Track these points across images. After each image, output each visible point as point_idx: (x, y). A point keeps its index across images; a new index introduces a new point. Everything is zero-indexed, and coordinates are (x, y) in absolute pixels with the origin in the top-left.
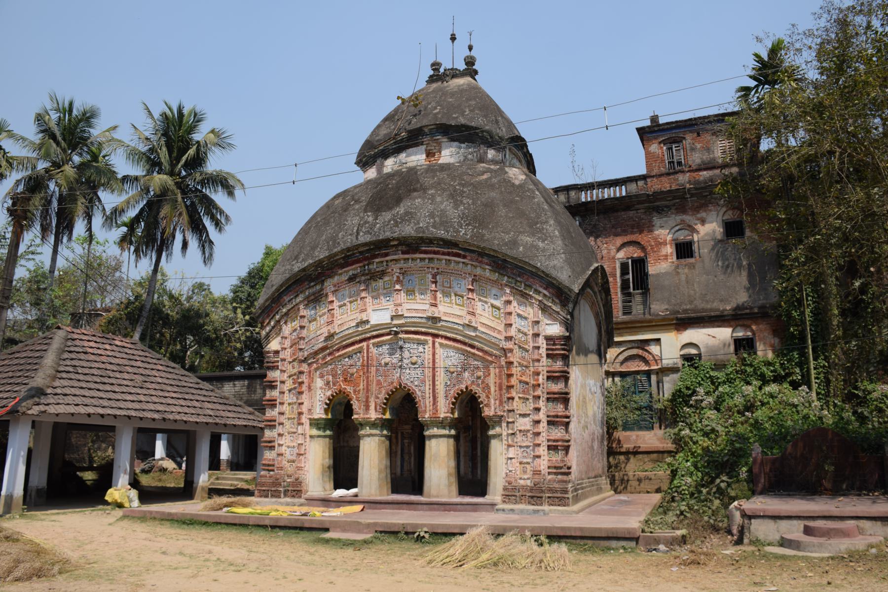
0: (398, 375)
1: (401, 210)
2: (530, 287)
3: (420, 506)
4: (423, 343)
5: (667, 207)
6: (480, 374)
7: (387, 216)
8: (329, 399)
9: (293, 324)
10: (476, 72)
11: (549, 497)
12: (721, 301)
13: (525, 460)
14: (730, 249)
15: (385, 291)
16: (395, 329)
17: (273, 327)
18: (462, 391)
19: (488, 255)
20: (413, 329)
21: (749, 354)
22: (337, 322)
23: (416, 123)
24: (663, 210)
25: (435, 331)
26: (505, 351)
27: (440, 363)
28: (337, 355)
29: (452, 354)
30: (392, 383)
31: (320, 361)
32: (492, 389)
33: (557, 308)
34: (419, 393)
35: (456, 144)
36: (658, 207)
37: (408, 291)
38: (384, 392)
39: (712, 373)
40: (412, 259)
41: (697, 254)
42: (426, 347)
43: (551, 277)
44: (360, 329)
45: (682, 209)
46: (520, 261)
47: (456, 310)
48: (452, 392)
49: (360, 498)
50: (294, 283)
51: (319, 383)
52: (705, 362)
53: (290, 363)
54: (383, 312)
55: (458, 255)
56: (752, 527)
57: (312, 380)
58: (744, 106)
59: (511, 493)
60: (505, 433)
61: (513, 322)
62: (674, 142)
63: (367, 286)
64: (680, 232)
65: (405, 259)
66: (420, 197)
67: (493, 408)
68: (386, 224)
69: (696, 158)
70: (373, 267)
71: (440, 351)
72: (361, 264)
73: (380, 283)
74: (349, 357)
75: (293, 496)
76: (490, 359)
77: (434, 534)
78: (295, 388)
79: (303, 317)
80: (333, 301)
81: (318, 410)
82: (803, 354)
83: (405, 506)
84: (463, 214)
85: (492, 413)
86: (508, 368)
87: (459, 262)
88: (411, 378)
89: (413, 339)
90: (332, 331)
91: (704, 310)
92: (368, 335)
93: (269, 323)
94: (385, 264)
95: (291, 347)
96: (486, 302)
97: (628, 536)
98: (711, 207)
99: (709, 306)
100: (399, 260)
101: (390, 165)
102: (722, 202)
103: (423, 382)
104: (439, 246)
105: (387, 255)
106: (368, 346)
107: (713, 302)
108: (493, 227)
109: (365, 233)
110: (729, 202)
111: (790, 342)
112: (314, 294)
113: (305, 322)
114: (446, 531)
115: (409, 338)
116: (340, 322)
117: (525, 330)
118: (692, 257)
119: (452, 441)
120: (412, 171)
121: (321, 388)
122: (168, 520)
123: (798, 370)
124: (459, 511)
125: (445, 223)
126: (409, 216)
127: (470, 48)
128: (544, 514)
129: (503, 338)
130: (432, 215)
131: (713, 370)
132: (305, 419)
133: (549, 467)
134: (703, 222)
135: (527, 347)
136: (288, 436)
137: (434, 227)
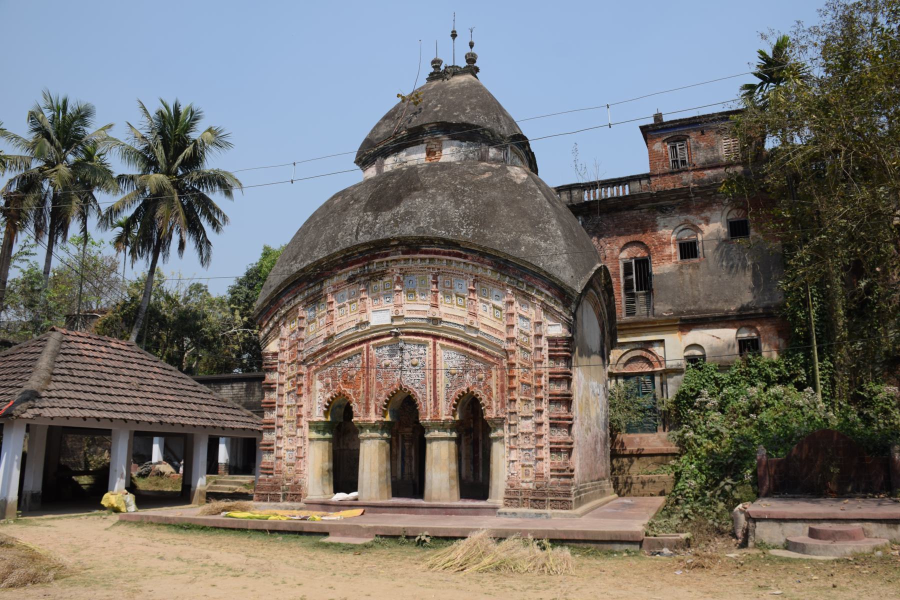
0: (398, 377)
1: (401, 209)
2: (532, 287)
3: (421, 510)
4: (424, 345)
5: (670, 206)
6: (482, 375)
7: (387, 215)
8: (329, 402)
9: (292, 325)
10: (477, 70)
11: (552, 501)
12: (726, 301)
13: (527, 463)
14: (734, 249)
15: (385, 292)
16: (395, 330)
17: (272, 329)
18: (463, 393)
19: (489, 255)
20: (413, 330)
21: (754, 355)
22: (336, 324)
23: (416, 122)
24: (666, 210)
25: (436, 332)
26: (507, 352)
27: (441, 365)
28: (337, 356)
29: (453, 356)
30: (393, 385)
31: (319, 363)
32: (494, 391)
33: (559, 309)
34: (420, 396)
35: (457, 142)
36: (662, 206)
37: (408, 292)
38: (384, 394)
39: (716, 375)
40: (413, 260)
41: (701, 254)
42: (427, 348)
43: (553, 278)
44: (360, 330)
45: (686, 208)
46: (522, 261)
47: (458, 311)
48: (453, 394)
49: (359, 502)
50: (294, 283)
51: (318, 385)
52: (710, 363)
53: (289, 365)
54: (383, 313)
55: (459, 255)
56: (757, 530)
57: (311, 382)
58: (749, 103)
59: (514, 497)
60: (506, 436)
61: (514, 323)
62: (678, 141)
63: (367, 287)
64: (684, 232)
65: (405, 260)
66: (420, 196)
67: (495, 411)
68: (385, 224)
69: (700, 157)
70: (373, 267)
71: (441, 353)
72: (361, 265)
73: (380, 284)
74: (348, 359)
75: (293, 500)
76: (491, 360)
77: (436, 538)
78: (294, 390)
79: (302, 318)
80: (332, 302)
81: (317, 413)
82: (808, 355)
83: (406, 509)
84: (465, 213)
85: (493, 416)
86: (510, 370)
87: (460, 263)
88: (412, 380)
89: (414, 341)
90: (331, 333)
91: (708, 311)
92: (368, 337)
93: (267, 325)
94: (385, 264)
95: (290, 349)
96: (488, 303)
97: (631, 539)
98: (715, 207)
99: (713, 307)
100: (400, 260)
101: (390, 163)
102: (726, 201)
103: (424, 384)
104: (439, 246)
105: (387, 255)
106: (368, 348)
107: (717, 302)
108: (494, 227)
109: (365, 233)
110: (734, 202)
111: (795, 343)
112: (313, 295)
113: (304, 324)
114: (447, 535)
115: (409, 340)
116: (339, 324)
117: (528, 331)
118: (696, 257)
119: (453, 443)
120: (413, 169)
121: (321, 390)
122: (165, 525)
123: (803, 371)
124: (461, 514)
125: (445, 223)
126: (409, 216)
127: (471, 45)
128: (547, 517)
129: (504, 340)
130: (433, 215)
131: (717, 371)
132: (304, 422)
133: (551, 470)
134: (707, 221)
135: (529, 348)
136: (287, 439)
137: (435, 226)
